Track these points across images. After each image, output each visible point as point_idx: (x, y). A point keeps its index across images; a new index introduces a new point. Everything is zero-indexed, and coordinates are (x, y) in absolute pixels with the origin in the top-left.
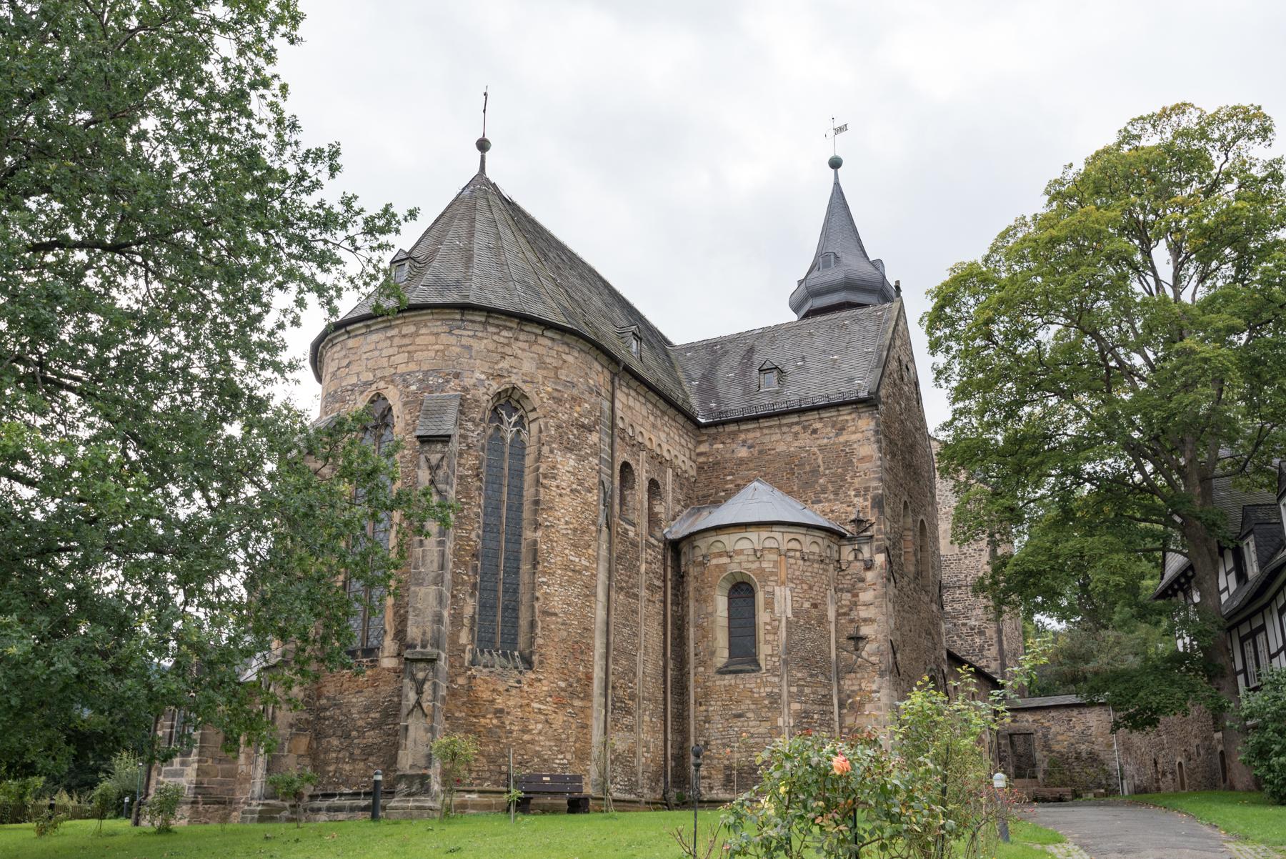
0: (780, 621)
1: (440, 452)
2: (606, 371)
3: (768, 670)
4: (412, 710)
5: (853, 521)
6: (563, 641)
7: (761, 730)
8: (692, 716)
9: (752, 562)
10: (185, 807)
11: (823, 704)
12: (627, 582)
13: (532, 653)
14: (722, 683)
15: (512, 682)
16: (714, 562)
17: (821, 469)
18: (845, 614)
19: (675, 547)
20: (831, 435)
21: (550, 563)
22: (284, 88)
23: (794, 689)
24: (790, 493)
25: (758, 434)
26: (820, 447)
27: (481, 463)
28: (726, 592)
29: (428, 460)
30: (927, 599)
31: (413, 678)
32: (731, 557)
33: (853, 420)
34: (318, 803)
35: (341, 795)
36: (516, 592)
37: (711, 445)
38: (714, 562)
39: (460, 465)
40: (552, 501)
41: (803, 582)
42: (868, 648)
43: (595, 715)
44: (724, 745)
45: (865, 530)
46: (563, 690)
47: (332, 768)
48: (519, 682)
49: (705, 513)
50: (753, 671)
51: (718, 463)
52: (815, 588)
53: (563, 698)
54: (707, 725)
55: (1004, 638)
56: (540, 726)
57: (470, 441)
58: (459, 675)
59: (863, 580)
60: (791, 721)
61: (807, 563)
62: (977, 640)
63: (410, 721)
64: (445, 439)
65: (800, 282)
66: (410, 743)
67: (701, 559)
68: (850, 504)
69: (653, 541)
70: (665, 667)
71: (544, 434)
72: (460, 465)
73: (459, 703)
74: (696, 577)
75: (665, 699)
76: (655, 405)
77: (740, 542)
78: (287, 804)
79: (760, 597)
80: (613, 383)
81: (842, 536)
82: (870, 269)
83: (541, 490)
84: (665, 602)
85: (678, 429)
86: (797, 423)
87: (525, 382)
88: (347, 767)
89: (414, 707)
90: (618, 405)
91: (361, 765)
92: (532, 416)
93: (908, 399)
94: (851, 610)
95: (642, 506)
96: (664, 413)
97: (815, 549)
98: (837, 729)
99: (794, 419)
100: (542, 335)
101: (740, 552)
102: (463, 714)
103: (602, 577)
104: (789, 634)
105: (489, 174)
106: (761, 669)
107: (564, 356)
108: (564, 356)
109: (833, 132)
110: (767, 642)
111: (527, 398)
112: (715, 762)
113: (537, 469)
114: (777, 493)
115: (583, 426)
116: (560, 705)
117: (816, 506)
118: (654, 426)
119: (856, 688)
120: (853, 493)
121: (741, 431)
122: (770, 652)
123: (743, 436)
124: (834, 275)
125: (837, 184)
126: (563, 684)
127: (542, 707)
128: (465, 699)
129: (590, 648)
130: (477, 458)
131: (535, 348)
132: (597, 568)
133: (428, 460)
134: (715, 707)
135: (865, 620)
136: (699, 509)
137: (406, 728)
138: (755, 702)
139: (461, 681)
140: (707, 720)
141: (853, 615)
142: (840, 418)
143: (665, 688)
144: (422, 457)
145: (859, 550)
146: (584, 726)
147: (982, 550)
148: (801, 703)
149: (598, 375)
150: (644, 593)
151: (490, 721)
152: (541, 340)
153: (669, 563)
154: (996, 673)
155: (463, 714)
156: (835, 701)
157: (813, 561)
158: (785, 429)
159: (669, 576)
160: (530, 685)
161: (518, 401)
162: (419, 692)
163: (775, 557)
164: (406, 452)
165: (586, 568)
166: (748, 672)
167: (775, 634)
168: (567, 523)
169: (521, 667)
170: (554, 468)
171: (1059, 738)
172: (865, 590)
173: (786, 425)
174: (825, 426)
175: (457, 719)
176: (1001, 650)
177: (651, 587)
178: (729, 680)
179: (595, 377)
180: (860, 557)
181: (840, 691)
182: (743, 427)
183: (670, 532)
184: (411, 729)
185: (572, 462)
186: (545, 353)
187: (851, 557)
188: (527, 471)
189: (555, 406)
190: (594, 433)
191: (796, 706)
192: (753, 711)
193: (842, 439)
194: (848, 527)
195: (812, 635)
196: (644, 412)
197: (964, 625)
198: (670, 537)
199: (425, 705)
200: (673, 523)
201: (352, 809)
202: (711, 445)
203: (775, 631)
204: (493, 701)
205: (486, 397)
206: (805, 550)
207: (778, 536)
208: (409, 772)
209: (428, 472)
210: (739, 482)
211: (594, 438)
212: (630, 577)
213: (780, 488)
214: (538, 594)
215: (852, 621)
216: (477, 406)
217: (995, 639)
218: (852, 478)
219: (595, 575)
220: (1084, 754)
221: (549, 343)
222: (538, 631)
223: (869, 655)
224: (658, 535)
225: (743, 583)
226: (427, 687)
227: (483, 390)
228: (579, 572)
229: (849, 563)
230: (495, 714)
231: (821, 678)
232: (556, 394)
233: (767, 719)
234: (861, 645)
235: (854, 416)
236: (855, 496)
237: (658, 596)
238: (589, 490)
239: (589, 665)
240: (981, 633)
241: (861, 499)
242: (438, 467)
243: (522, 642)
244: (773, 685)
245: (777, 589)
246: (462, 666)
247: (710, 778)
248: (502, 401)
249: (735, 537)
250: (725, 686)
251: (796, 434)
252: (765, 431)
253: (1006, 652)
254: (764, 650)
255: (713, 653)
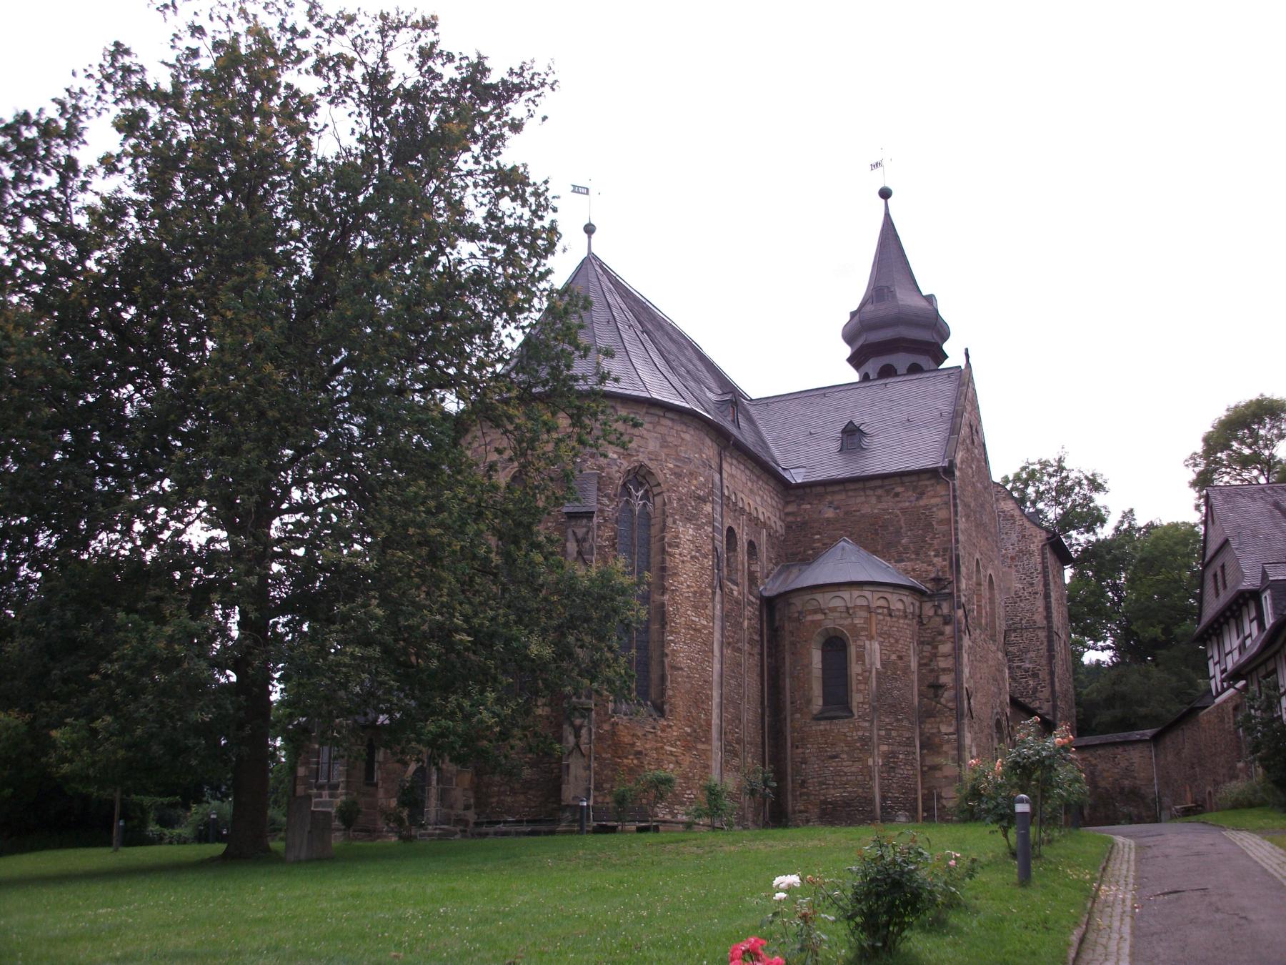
0: (871, 672)
1: (585, 526)
2: (715, 445)
3: (860, 716)
4: (572, 751)
5: (933, 579)
6: (688, 692)
7: (853, 769)
8: (789, 758)
9: (845, 618)
10: (337, 834)
11: (907, 745)
12: (732, 638)
13: (663, 703)
14: (818, 728)
15: (648, 728)
16: (809, 618)
17: (903, 530)
18: (925, 665)
19: (770, 605)
20: (912, 499)
21: (676, 623)
22: (353, 132)
23: (883, 733)
24: (875, 552)
25: (843, 496)
26: (904, 511)
27: (616, 534)
28: (820, 646)
29: (574, 533)
30: (994, 648)
31: (572, 724)
32: (825, 614)
33: (932, 485)
34: (484, 829)
35: (505, 822)
36: (646, 648)
37: (799, 505)
38: (809, 618)
39: (598, 536)
40: (676, 567)
41: (890, 636)
42: (946, 695)
43: (714, 756)
44: (821, 783)
45: (945, 587)
46: (689, 735)
47: (494, 800)
48: (654, 728)
49: (795, 571)
50: (847, 717)
51: (804, 523)
52: (901, 642)
53: (689, 742)
54: (804, 766)
55: (1056, 680)
56: (672, 766)
57: (606, 514)
58: (605, 722)
59: (942, 633)
60: (880, 761)
61: (894, 619)
62: (1031, 682)
63: (570, 760)
64: (589, 515)
65: (853, 314)
66: (571, 778)
67: (796, 615)
68: (930, 563)
69: (752, 598)
70: (763, 715)
71: (668, 507)
72: (598, 537)
73: (605, 746)
74: (792, 632)
75: (763, 743)
76: (752, 471)
77: (834, 601)
78: (458, 829)
79: (853, 650)
80: (720, 455)
81: (922, 593)
82: (924, 304)
83: (667, 558)
84: (761, 654)
85: (770, 492)
86: (881, 487)
87: (651, 460)
88: (509, 799)
89: (574, 748)
90: (725, 475)
91: (522, 797)
92: (656, 490)
93: (979, 461)
94: (931, 661)
95: (743, 567)
96: (758, 477)
97: (900, 606)
98: (919, 768)
99: (878, 483)
100: (664, 416)
101: (833, 610)
102: (609, 756)
103: (717, 635)
104: (879, 683)
105: (593, 250)
106: (853, 715)
107: (683, 435)
108: (683, 435)
109: (884, 163)
110: (859, 691)
111: (652, 474)
112: (812, 797)
113: (663, 538)
114: (863, 552)
115: (699, 498)
116: (688, 748)
117: (898, 565)
118: (751, 491)
119: (935, 731)
120: (933, 553)
121: (827, 493)
122: (861, 700)
123: (829, 498)
124: (883, 310)
125: (887, 215)
126: (688, 730)
127: (673, 749)
128: (610, 743)
129: (710, 698)
130: (612, 530)
131: (659, 429)
132: (713, 628)
133: (574, 533)
134: (810, 749)
135: (944, 670)
136: (788, 567)
137: (568, 766)
138: (848, 744)
139: (606, 727)
140: (804, 761)
141: (933, 665)
142: (921, 483)
143: (763, 733)
144: (570, 531)
145: (939, 607)
146: (707, 767)
147: (1036, 593)
148: (888, 744)
149: (709, 450)
150: (747, 647)
151: (631, 761)
152: (664, 421)
153: (765, 618)
154: (1048, 714)
155: (609, 756)
156: (918, 743)
157: (898, 617)
158: (869, 492)
159: (765, 631)
160: (663, 731)
161: (644, 477)
162: (577, 736)
163: (864, 614)
164: (549, 524)
165: (705, 627)
166: (842, 718)
167: (866, 683)
168: (688, 587)
169: (655, 716)
170: (677, 537)
171: (1105, 774)
172: (943, 642)
173: (871, 488)
174: (907, 490)
175: (605, 759)
176: (1053, 692)
177: (751, 641)
178: (823, 725)
179: (707, 452)
180: (940, 612)
181: (921, 734)
182: (830, 489)
183: (765, 589)
184: (572, 767)
185: (691, 531)
186: (666, 432)
187: (931, 613)
188: (653, 540)
189: (676, 481)
190: (708, 504)
191: (884, 748)
192: (847, 753)
193: (922, 503)
194: (928, 585)
195: (898, 684)
196: (744, 479)
197: (1019, 667)
198: (766, 594)
199: (583, 747)
200: (766, 580)
201: (518, 834)
202: (799, 505)
203: (866, 681)
204: (633, 745)
205: (618, 474)
206: (892, 607)
207: (868, 594)
208: (572, 803)
209: (575, 544)
210: (826, 541)
211: (708, 508)
212: (735, 633)
213: (865, 548)
214: (666, 651)
215: (932, 671)
216: (611, 483)
217: (1047, 682)
218: (932, 539)
219: (712, 633)
220: (1126, 790)
221: (669, 423)
222: (668, 683)
223: (948, 701)
224: (755, 592)
225: (836, 637)
226: (584, 732)
227: (616, 468)
228: (699, 631)
229: (930, 618)
230: (635, 755)
231: (905, 723)
232: (677, 470)
233: (860, 760)
234: (940, 692)
235: (932, 481)
236: (935, 556)
237: (756, 650)
238: (705, 556)
239: (708, 713)
240: (1035, 675)
241: (940, 559)
242: (584, 540)
243: (653, 693)
244: (864, 729)
245: (867, 643)
246: (606, 713)
247: (806, 812)
248: (630, 477)
249: (829, 595)
250: (821, 731)
251: (879, 497)
252: (850, 494)
253: (1057, 694)
254: (856, 698)
255: (809, 702)
